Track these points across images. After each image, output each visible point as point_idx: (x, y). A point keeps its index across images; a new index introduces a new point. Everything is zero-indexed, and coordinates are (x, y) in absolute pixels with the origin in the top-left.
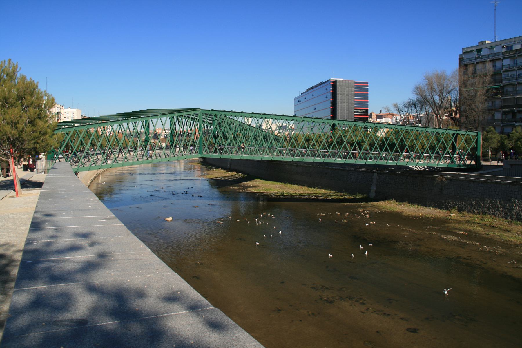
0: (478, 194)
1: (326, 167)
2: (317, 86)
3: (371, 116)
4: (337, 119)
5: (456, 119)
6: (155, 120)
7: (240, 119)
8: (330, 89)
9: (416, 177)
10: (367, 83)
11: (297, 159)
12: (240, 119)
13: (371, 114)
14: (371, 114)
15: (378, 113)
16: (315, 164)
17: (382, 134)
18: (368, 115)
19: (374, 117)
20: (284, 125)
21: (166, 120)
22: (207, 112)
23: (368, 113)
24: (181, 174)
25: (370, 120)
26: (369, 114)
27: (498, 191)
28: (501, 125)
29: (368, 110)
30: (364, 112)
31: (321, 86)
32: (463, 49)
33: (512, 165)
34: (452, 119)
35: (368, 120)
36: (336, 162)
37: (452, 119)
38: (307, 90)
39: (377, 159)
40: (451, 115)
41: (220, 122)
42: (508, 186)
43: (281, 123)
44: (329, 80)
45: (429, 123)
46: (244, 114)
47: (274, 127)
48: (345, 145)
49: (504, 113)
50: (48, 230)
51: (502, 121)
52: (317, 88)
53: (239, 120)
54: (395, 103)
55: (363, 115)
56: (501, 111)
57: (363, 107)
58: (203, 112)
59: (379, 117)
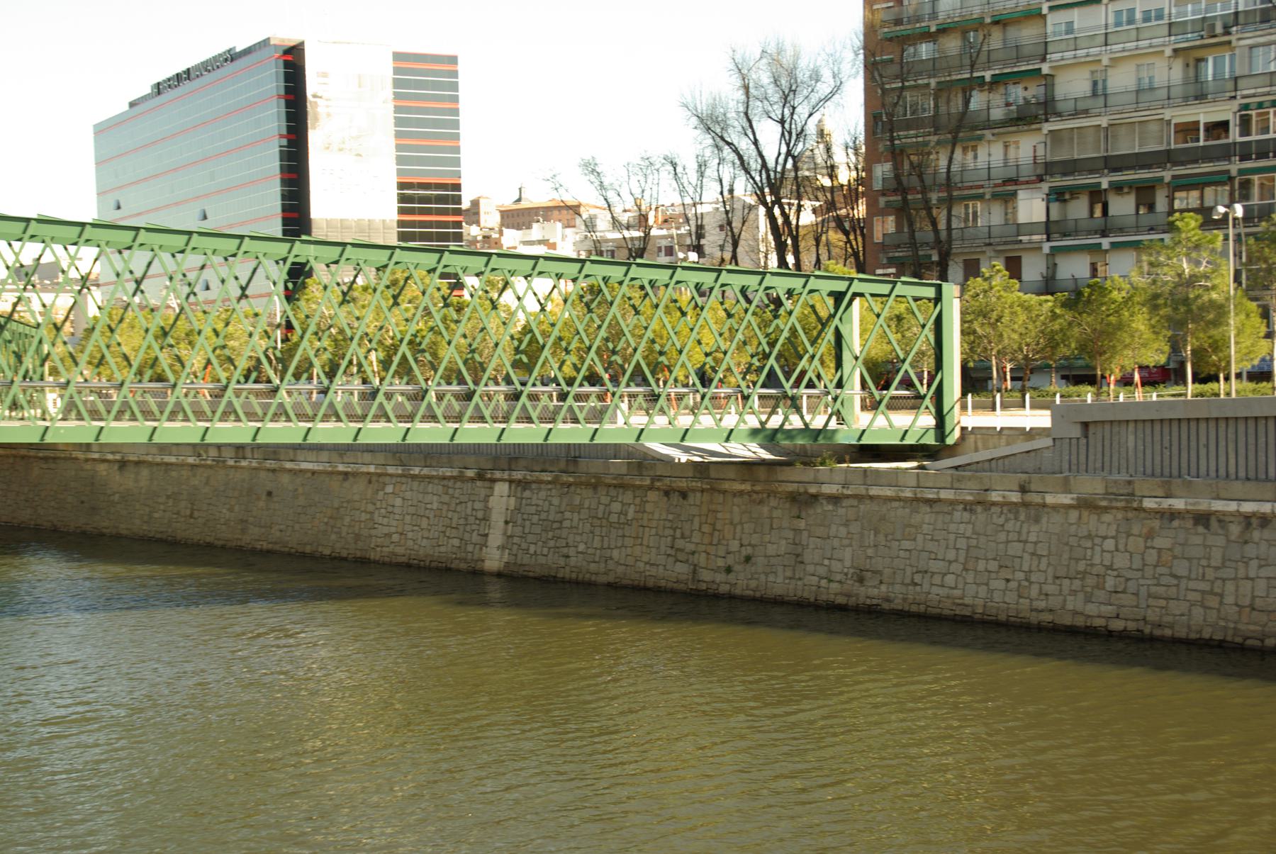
0: (951, 555)
1: (270, 464)
3: (473, 214)
4: (317, 234)
8: (271, 81)
9: (684, 495)
10: (453, 60)
13: (475, 203)
14: (475, 203)
15: (508, 202)
16: (213, 453)
18: (458, 212)
19: (490, 218)
20: (47, 258)
23: (458, 200)
25: (472, 231)
26: (465, 205)
27: (1033, 538)
28: (1046, 248)
29: (457, 187)
30: (440, 199)
31: (230, 67)
33: (1086, 425)
34: (839, 222)
35: (458, 237)
37: (839, 222)
38: (159, 89)
40: (831, 205)
41: (753, 560)
42: (1074, 515)
44: (265, 43)
45: (735, 244)
49: (1058, 196)
50: (699, 139)
51: (1050, 228)
52: (208, 78)
54: (588, 157)
55: (432, 210)
56: (1045, 187)
59: (517, 217)
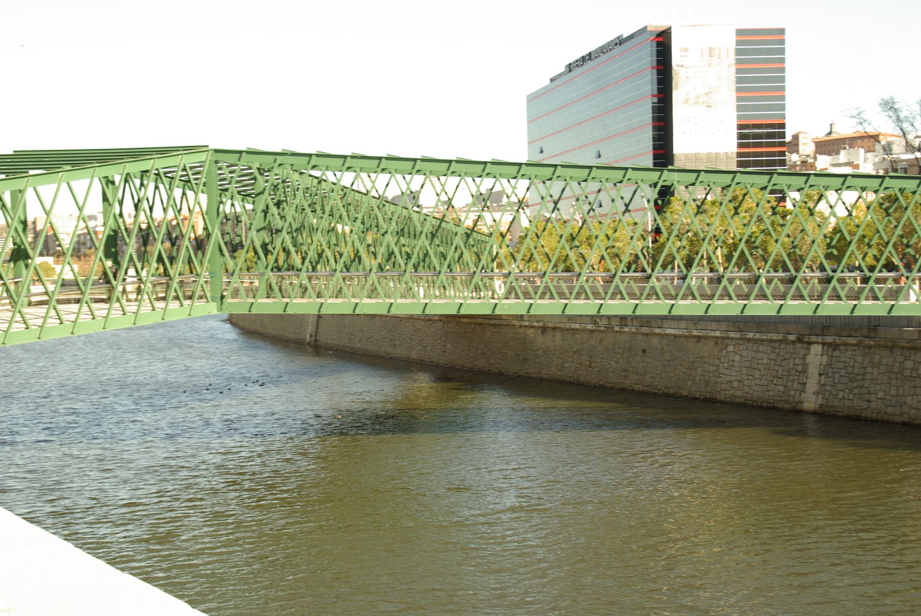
1: (644, 330)
2: (603, 50)
3: (794, 145)
4: (678, 164)
6: (47, 190)
7: (347, 179)
8: (647, 56)
10: (782, 31)
11: (546, 307)
12: (347, 179)
13: (796, 137)
14: (796, 137)
15: (821, 135)
18: (783, 144)
19: (807, 148)
20: (497, 188)
21: (87, 186)
23: (783, 135)
24: (177, 325)
25: (794, 158)
26: (788, 138)
29: (783, 126)
30: (769, 136)
31: (619, 49)
32: (740, 32)
35: (783, 163)
36: (675, 312)
38: (570, 68)
39: (820, 297)
46: (346, 161)
48: (742, 252)
52: (604, 57)
55: (763, 143)
58: (220, 156)
59: (828, 146)
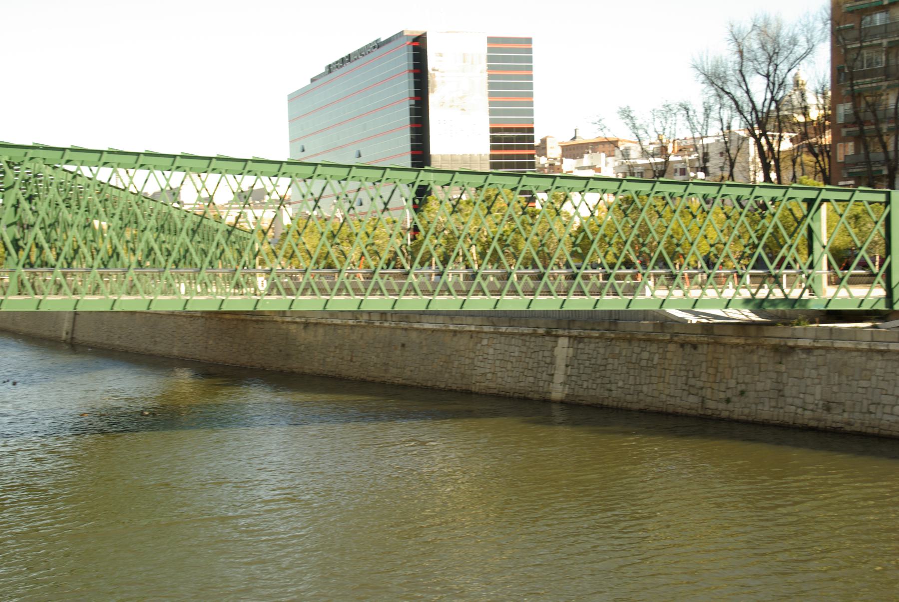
2: (362, 52)
3: (542, 149)
5: (823, 148)
8: (404, 60)
9: (695, 346)
12: (103, 174)
13: (544, 141)
14: (544, 141)
15: (567, 139)
17: (582, 207)
18: (532, 147)
19: (554, 151)
22: (18, 154)
23: (531, 139)
25: (542, 161)
26: (537, 142)
29: (531, 130)
30: (519, 139)
31: (377, 52)
34: (810, 147)
35: (532, 165)
37: (810, 147)
38: (330, 69)
40: (805, 136)
41: (747, 394)
43: (247, 181)
44: (401, 34)
45: (732, 165)
47: (224, 196)
52: (363, 60)
53: (99, 178)
54: (624, 106)
57: (514, 121)
59: (573, 150)
